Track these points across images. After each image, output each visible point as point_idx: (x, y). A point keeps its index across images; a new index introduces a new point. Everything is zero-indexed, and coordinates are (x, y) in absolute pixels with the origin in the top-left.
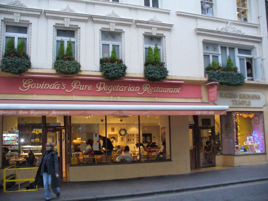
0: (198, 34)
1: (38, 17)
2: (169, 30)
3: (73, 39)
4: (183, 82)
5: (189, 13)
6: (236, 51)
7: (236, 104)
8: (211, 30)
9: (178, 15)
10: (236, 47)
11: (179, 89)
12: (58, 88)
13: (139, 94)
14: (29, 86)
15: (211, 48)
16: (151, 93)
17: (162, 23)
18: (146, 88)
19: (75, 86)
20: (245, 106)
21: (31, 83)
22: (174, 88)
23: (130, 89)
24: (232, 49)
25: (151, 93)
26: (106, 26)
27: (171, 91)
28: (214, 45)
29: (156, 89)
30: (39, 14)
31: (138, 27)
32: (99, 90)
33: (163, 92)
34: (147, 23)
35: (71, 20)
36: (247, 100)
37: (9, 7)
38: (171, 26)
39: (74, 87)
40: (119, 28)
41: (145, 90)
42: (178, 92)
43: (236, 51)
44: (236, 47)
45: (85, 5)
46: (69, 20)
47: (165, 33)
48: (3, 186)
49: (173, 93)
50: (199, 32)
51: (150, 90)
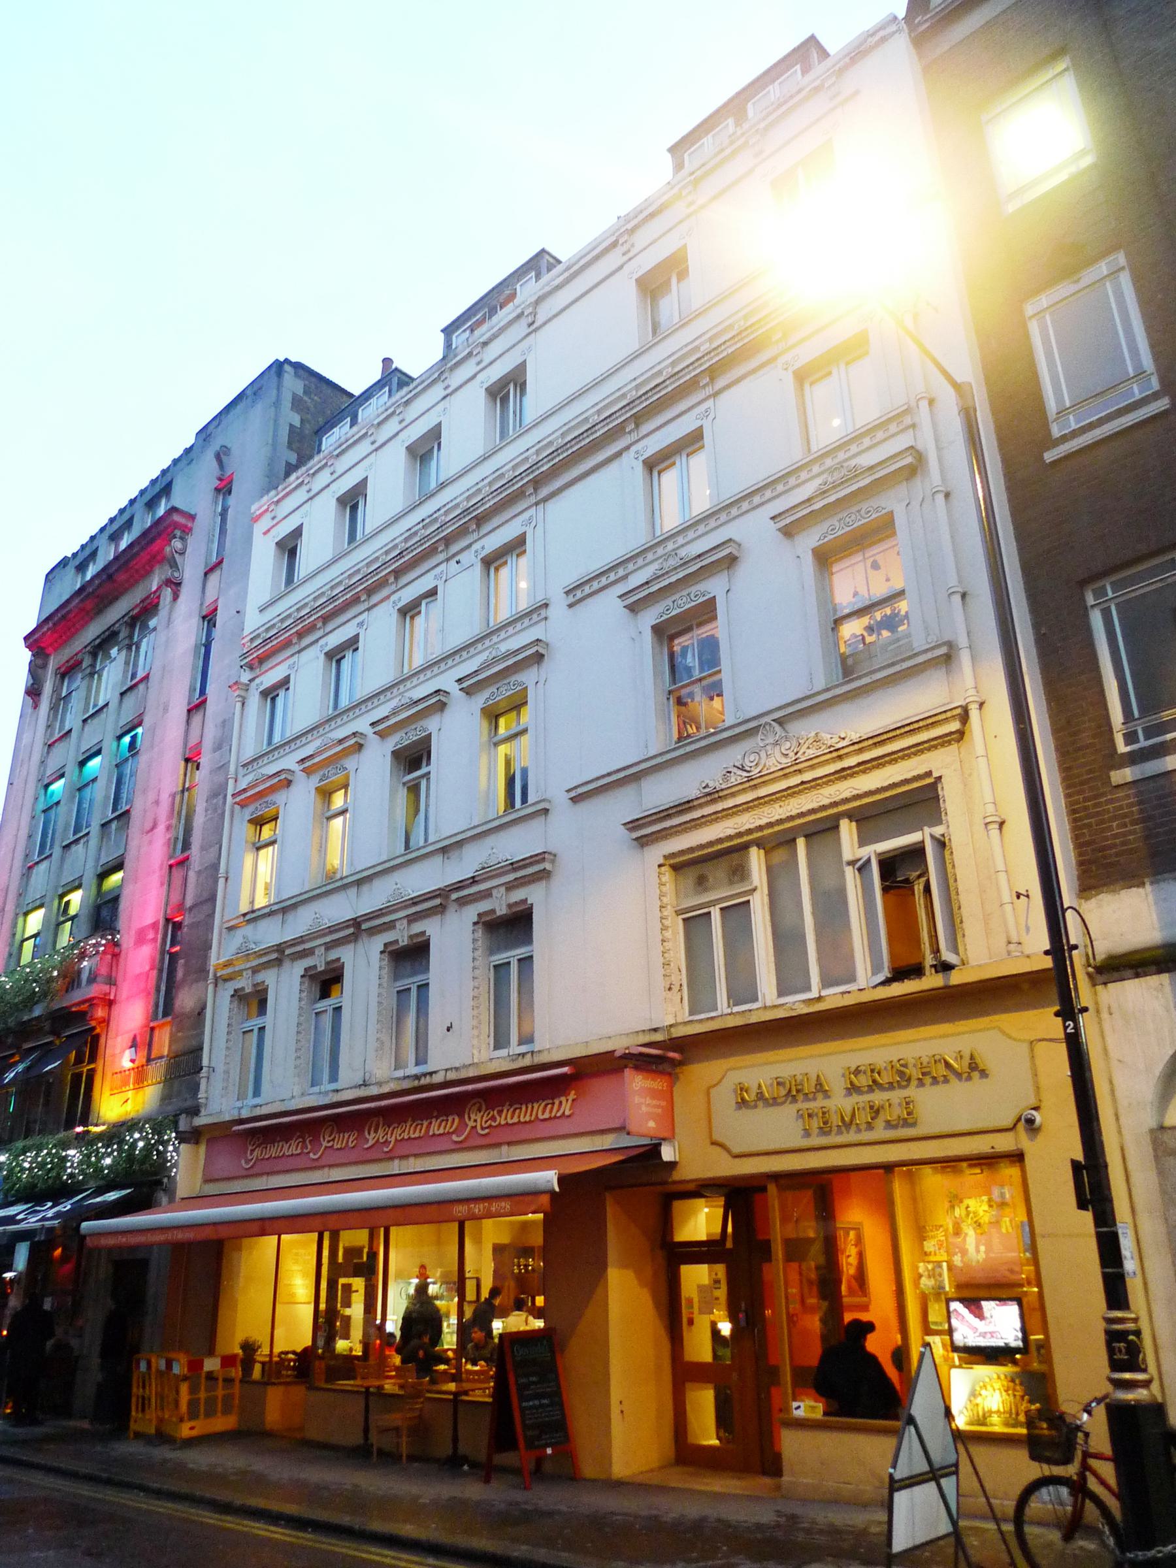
0: (643, 842)
1: (441, 909)
2: (544, 875)
3: (938, 831)
4: (565, 1070)
5: (603, 776)
6: (848, 830)
7: (824, 1131)
8: (531, 857)
9: (574, 800)
10: (745, 847)
11: (572, 1096)
12: (299, 1151)
13: (456, 1142)
14: (255, 1153)
15: (717, 873)
16: (486, 1131)
17: (512, 864)
18: (473, 1117)
19: (327, 1138)
20: (880, 1133)
21: (259, 1146)
22: (553, 1099)
23: (436, 1128)
24: (821, 829)
25: (486, 1131)
26: (484, 906)
27: (543, 1113)
28: (728, 857)
29: (500, 1113)
30: (955, 726)
31: (463, 902)
32: (370, 1143)
33: (519, 1122)
34: (474, 881)
35: (410, 922)
36: (896, 1096)
37: (721, 794)
38: (539, 858)
39: (325, 1144)
40: (517, 895)
41: (471, 1124)
42: (567, 1113)
43: (848, 830)
44: (838, 817)
45: (438, 859)
46: (503, 889)
47: (534, 895)
48: (452, 1499)
49: (550, 1118)
50: (644, 831)
51: (485, 1119)
